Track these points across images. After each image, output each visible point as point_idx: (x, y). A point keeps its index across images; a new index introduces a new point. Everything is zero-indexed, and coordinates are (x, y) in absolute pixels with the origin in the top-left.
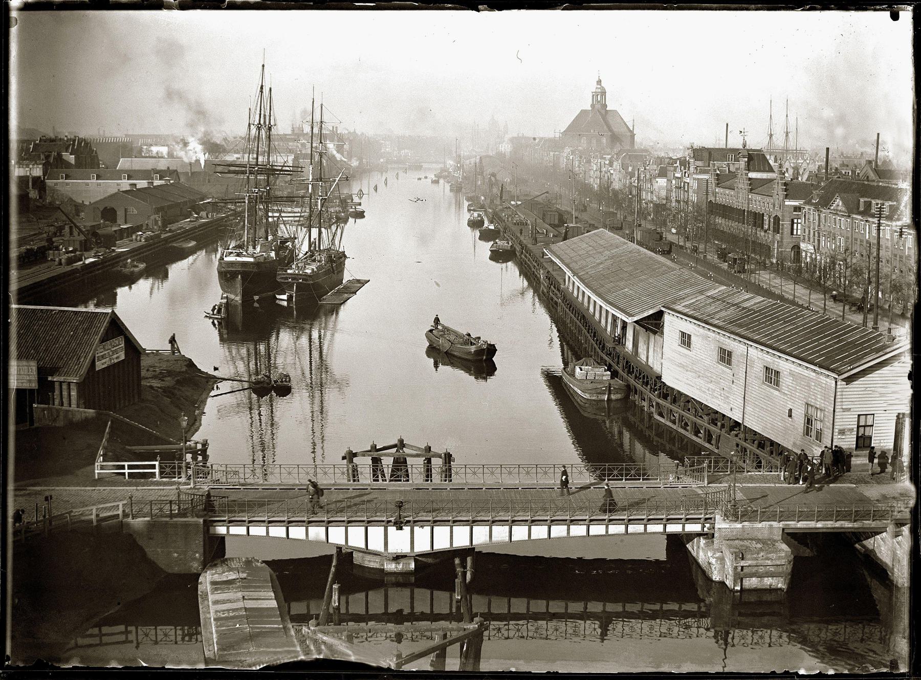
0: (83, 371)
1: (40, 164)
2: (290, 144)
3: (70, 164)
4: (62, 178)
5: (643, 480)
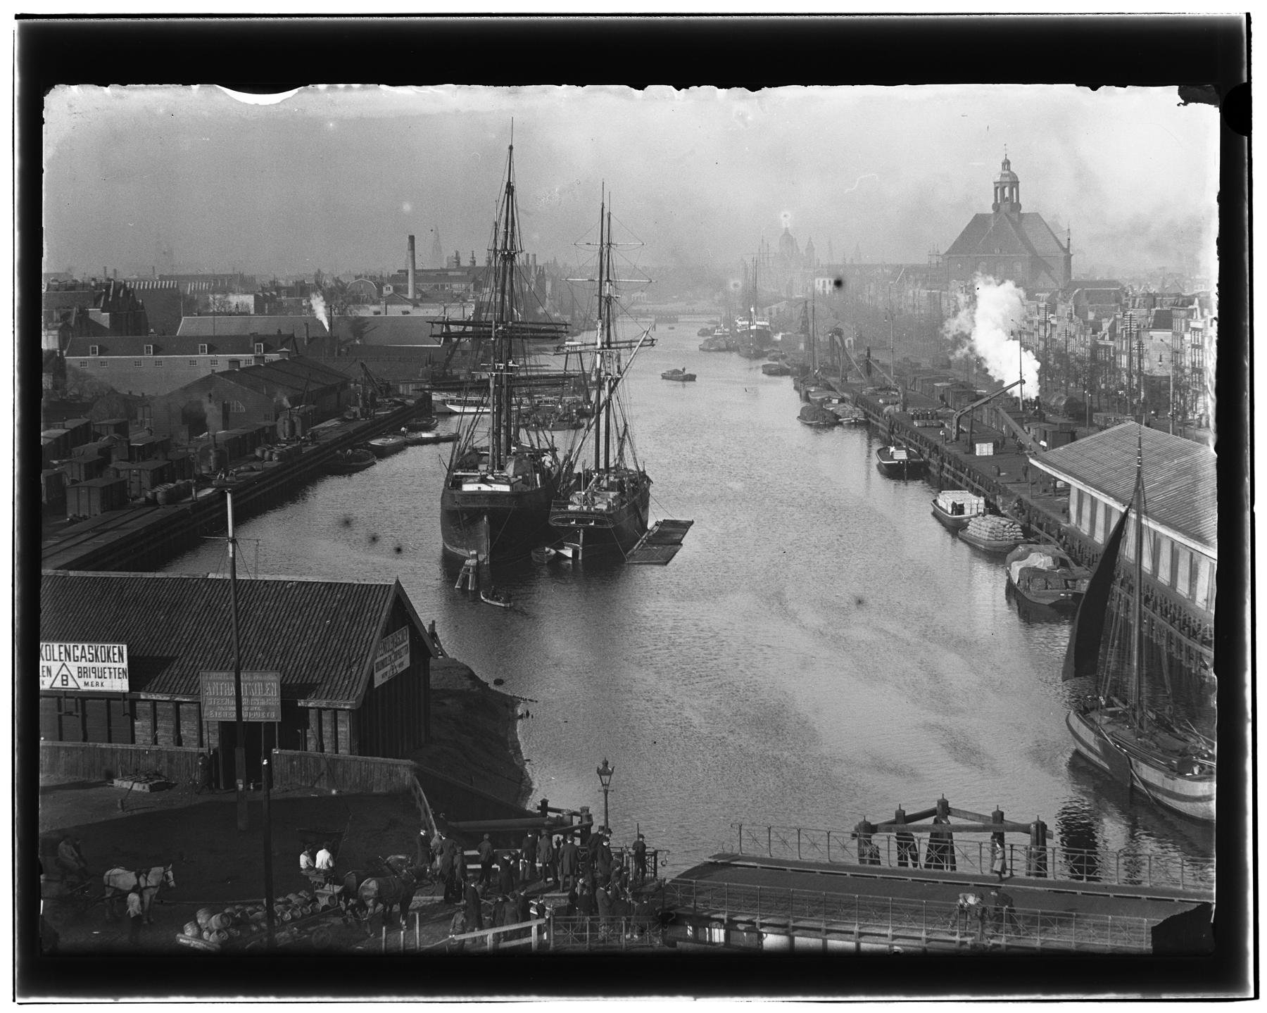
0: (360, 690)
1: (55, 328)
2: (455, 286)
3: (101, 327)
4: (94, 352)
5: (1089, 879)
